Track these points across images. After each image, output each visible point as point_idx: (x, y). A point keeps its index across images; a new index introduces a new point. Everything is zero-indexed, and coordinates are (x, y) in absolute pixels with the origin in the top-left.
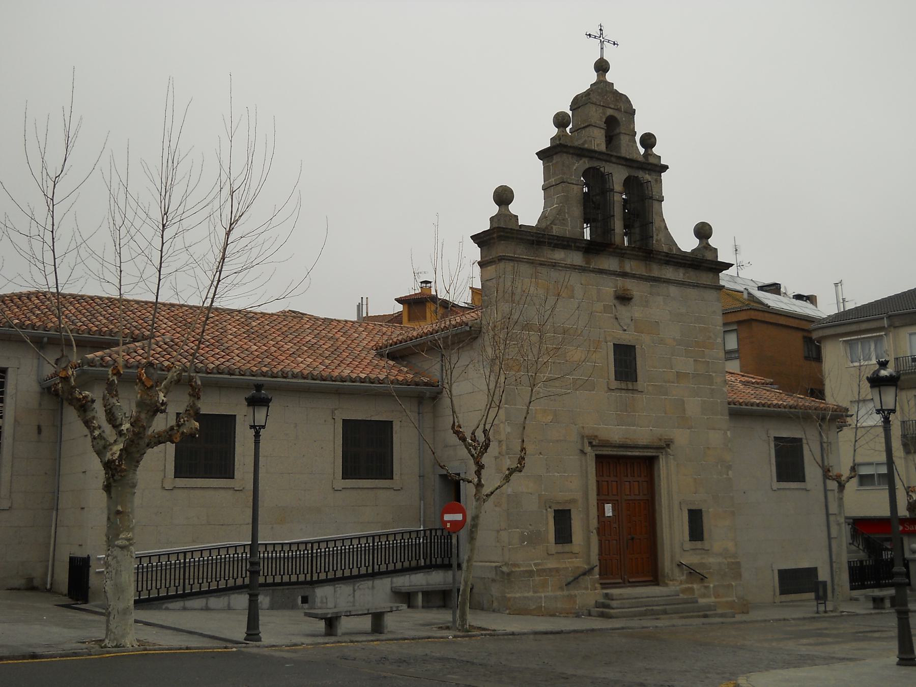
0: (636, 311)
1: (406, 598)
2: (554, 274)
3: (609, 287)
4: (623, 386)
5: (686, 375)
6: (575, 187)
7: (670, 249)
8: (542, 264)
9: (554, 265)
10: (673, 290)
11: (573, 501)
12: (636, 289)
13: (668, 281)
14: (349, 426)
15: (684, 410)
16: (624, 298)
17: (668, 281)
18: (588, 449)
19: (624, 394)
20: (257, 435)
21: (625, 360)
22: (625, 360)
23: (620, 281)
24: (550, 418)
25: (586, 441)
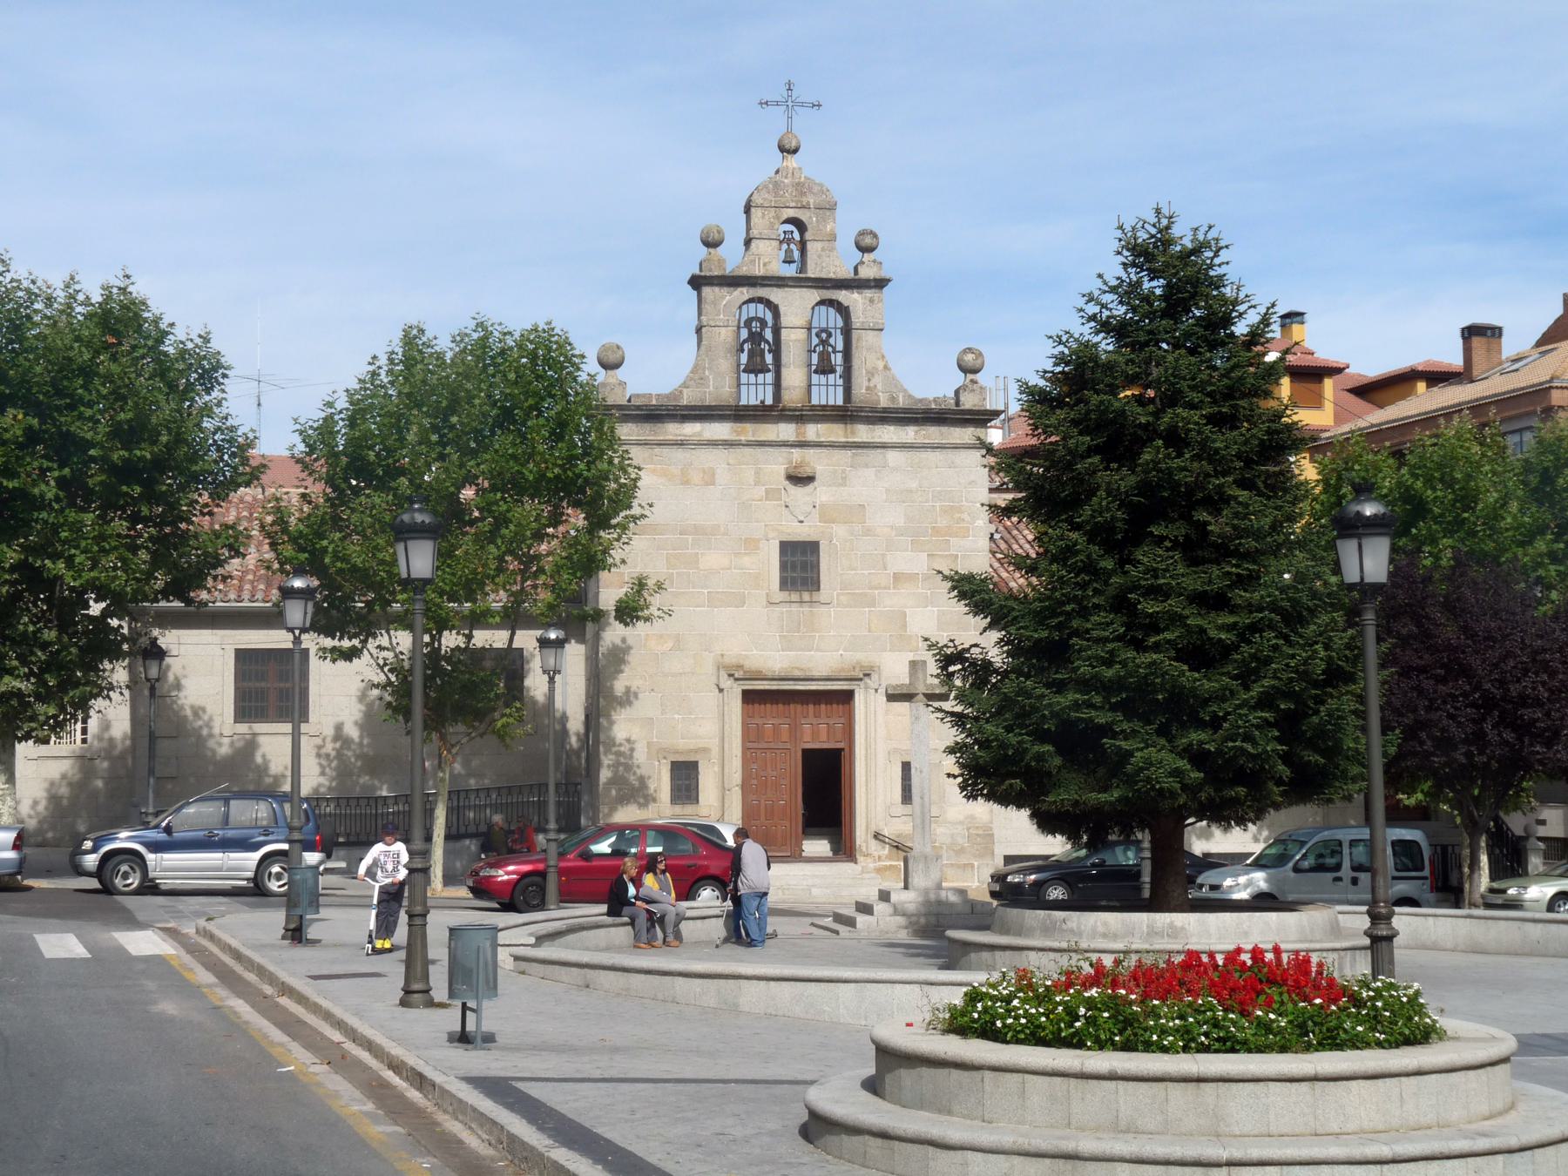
0: (820, 493)
1: (1514, 614)
2: (679, 454)
3: (776, 465)
4: (795, 596)
5: (911, 577)
6: (723, 330)
7: (893, 399)
8: (660, 444)
9: (681, 444)
10: (893, 456)
11: (706, 750)
12: (817, 461)
13: (884, 446)
14: (243, 656)
15: (904, 626)
16: (800, 479)
17: (884, 446)
18: (727, 683)
19: (795, 608)
20: (552, 680)
21: (800, 565)
22: (800, 565)
23: (797, 454)
24: (670, 644)
25: (724, 675)
